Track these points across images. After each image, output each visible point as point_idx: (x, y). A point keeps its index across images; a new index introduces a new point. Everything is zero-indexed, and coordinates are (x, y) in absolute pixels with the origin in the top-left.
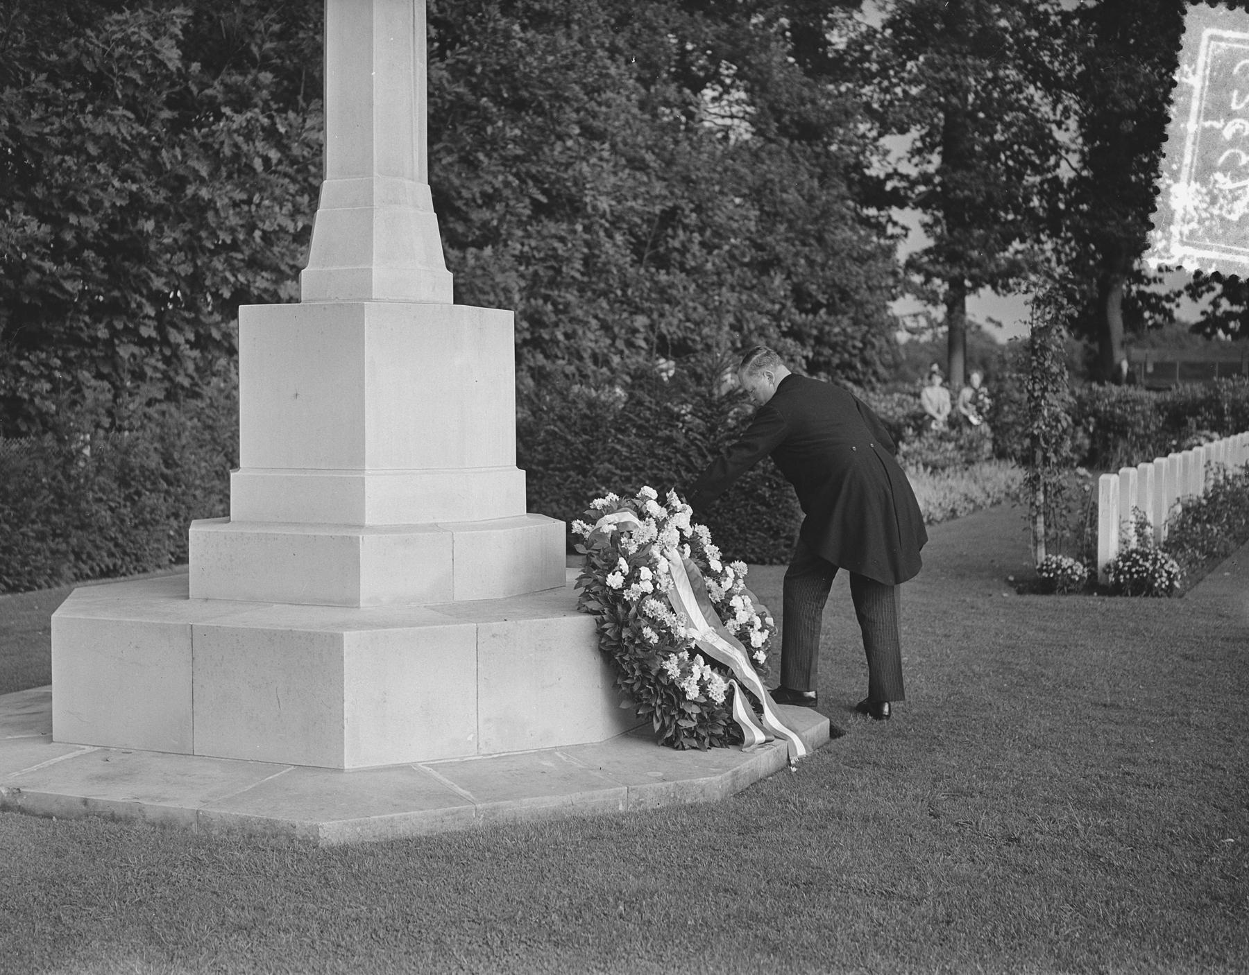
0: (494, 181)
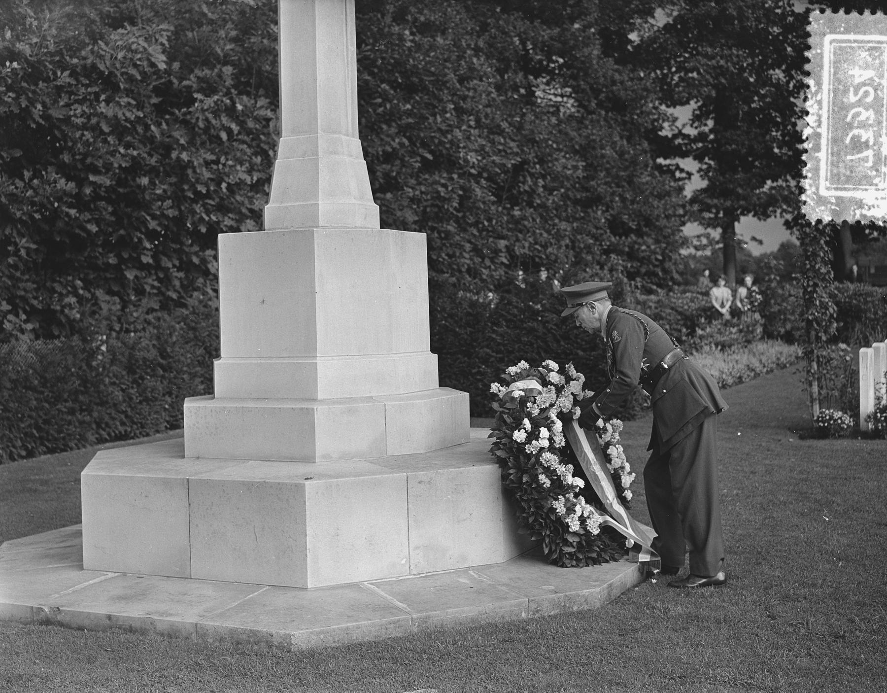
0: (392, 143)
